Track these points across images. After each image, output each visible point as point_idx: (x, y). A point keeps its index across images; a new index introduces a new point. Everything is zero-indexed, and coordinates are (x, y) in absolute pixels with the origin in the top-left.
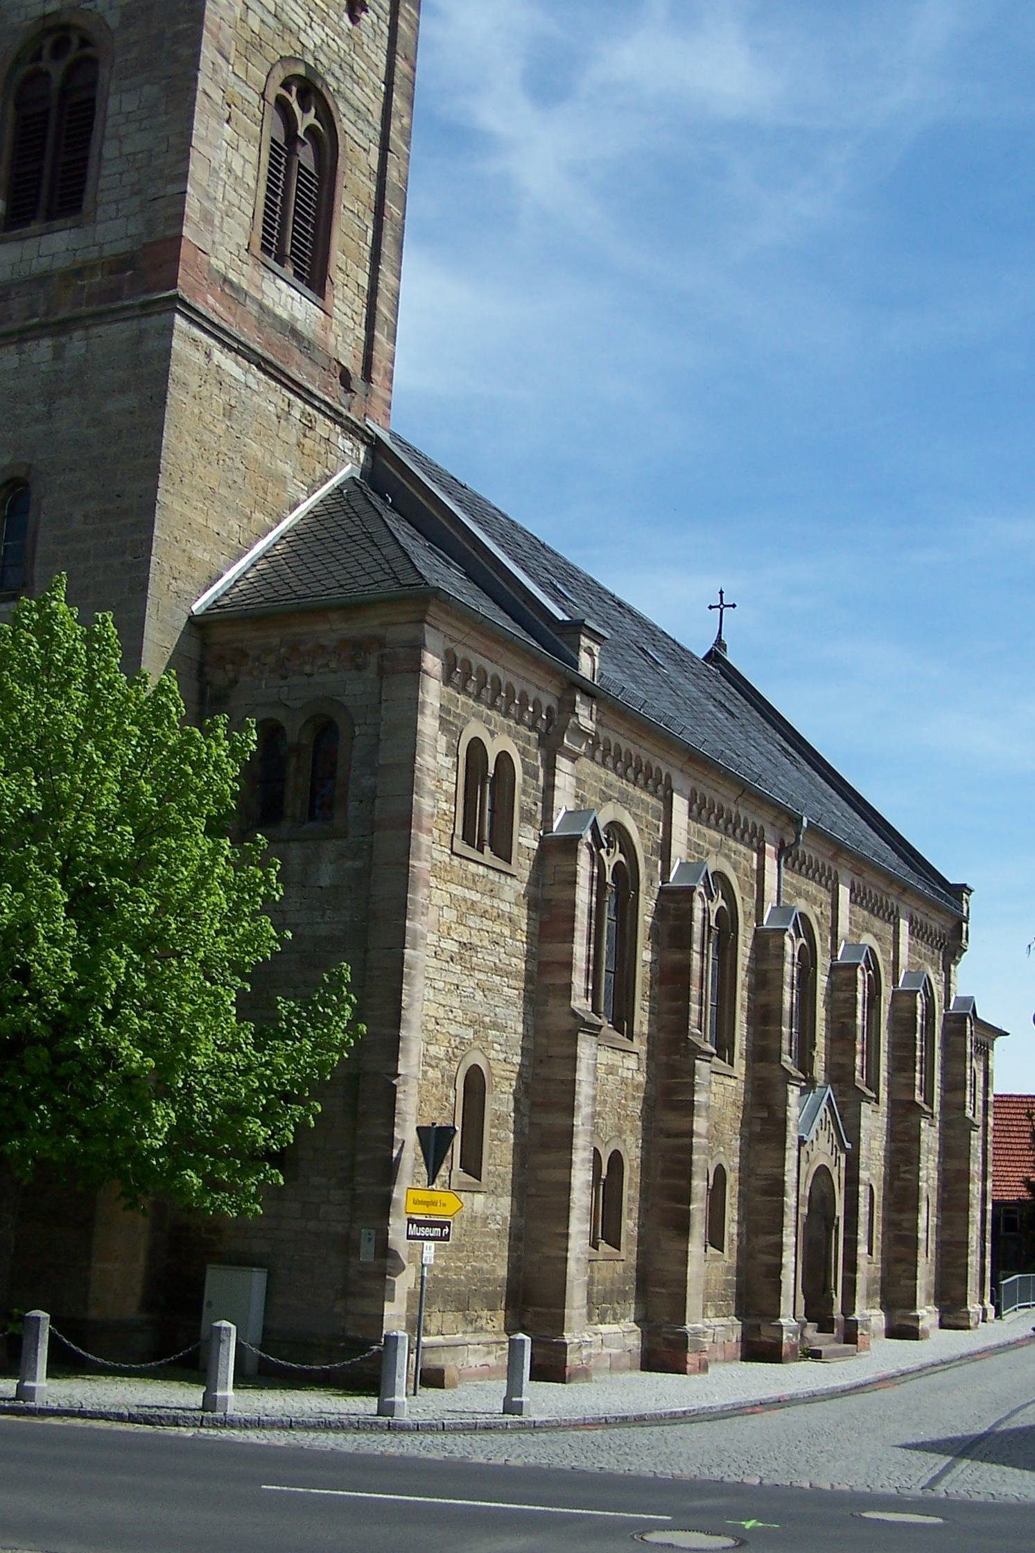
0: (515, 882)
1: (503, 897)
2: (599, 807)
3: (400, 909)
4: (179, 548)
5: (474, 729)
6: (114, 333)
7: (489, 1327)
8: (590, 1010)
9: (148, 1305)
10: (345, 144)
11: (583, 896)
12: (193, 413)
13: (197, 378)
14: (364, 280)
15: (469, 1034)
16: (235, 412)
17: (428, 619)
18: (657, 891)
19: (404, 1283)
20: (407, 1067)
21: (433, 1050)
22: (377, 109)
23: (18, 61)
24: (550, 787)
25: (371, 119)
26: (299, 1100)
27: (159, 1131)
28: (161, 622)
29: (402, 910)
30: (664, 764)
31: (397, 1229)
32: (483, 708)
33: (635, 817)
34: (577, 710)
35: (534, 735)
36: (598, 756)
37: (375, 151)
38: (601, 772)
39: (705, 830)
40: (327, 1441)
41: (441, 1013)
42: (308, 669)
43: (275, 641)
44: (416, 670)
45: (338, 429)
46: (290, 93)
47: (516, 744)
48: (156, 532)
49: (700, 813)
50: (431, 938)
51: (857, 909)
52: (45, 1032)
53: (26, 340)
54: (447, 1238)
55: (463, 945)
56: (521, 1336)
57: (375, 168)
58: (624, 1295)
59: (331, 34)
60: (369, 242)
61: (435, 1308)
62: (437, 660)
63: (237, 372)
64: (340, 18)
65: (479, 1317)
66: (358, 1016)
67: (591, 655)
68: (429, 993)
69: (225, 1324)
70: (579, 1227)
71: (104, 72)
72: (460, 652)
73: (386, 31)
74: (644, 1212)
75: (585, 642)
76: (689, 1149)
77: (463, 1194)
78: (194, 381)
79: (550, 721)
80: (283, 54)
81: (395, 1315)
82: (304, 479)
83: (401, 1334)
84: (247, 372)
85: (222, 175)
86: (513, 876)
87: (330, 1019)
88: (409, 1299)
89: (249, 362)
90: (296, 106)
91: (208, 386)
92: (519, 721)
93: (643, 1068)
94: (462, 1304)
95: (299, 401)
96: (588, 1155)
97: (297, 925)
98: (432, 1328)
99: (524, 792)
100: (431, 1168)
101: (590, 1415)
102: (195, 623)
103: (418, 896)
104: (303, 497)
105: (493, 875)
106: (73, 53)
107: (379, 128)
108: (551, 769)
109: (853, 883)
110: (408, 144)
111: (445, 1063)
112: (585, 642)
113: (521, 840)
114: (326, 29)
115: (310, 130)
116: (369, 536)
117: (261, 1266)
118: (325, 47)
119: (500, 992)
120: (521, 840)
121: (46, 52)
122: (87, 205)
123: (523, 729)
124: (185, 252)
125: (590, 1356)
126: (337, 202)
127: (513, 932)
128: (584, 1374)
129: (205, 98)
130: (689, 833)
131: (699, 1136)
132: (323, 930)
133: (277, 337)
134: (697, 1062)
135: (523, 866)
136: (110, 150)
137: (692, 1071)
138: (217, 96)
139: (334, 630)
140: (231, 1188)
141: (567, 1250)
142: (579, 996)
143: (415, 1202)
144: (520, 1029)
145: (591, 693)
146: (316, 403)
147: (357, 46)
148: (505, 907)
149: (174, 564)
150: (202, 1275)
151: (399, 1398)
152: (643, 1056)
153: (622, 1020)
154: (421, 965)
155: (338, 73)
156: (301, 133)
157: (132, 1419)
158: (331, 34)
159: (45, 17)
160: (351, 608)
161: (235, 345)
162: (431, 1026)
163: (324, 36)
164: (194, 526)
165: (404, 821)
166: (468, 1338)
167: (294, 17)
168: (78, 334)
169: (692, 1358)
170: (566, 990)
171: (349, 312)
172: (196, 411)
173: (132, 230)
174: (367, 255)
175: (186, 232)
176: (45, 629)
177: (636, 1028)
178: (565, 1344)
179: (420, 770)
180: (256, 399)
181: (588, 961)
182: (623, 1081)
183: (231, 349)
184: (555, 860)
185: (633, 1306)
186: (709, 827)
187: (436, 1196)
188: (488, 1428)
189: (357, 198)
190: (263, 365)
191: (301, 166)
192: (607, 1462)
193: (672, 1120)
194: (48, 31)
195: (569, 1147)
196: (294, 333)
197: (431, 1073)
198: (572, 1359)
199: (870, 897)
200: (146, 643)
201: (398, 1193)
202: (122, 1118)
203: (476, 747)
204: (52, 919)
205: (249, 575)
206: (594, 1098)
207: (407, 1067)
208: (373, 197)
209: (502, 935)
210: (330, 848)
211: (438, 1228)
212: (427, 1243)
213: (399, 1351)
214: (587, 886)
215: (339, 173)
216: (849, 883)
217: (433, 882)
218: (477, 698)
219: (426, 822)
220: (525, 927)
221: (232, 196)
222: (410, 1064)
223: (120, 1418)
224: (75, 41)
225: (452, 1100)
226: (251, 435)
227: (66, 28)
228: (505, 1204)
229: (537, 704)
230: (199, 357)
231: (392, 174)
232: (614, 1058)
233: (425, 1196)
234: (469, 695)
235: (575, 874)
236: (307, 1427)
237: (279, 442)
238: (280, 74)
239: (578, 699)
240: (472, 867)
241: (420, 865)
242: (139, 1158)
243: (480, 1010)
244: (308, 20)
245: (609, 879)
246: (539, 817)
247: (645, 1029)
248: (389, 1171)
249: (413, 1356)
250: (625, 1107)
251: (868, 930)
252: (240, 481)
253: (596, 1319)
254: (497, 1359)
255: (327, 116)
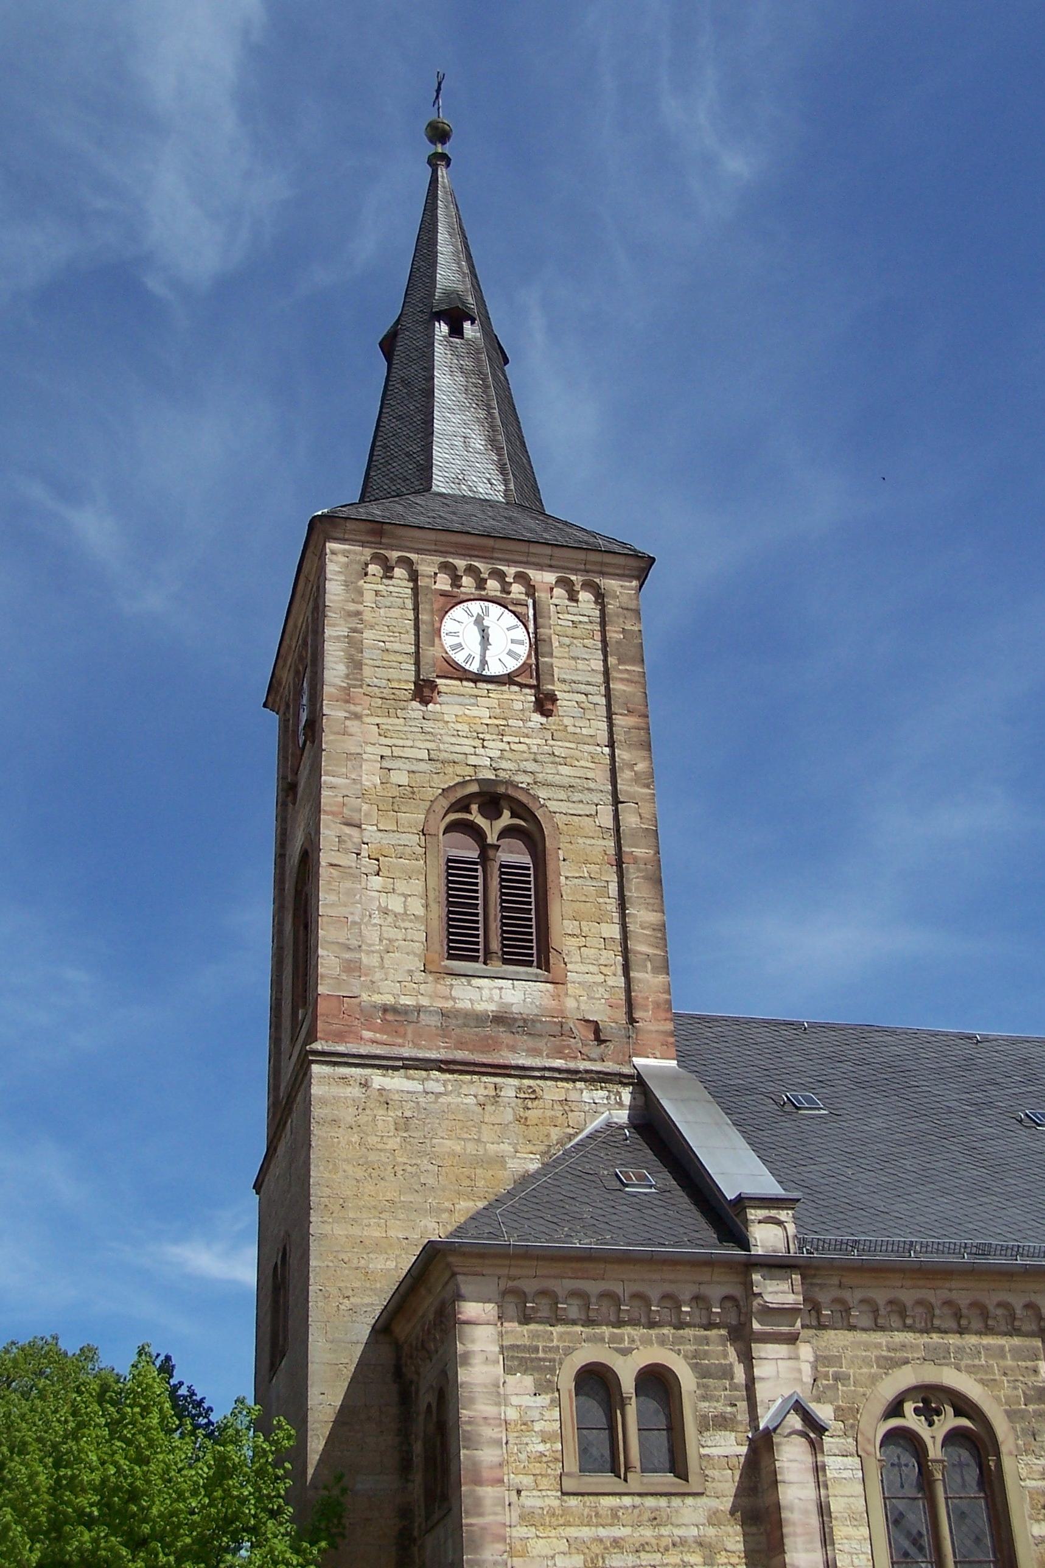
4: (350, 1268)
12: (349, 1143)
17: (456, 1269)
28: (332, 1342)
47: (679, 1352)
48: (313, 1263)
78: (348, 1115)
82: (534, 1149)
89: (426, 1070)
91: (368, 1112)
133: (469, 1033)
146: (537, 1074)
149: (342, 1285)
164: (367, 1242)
183: (396, 1068)
255: (521, 810)
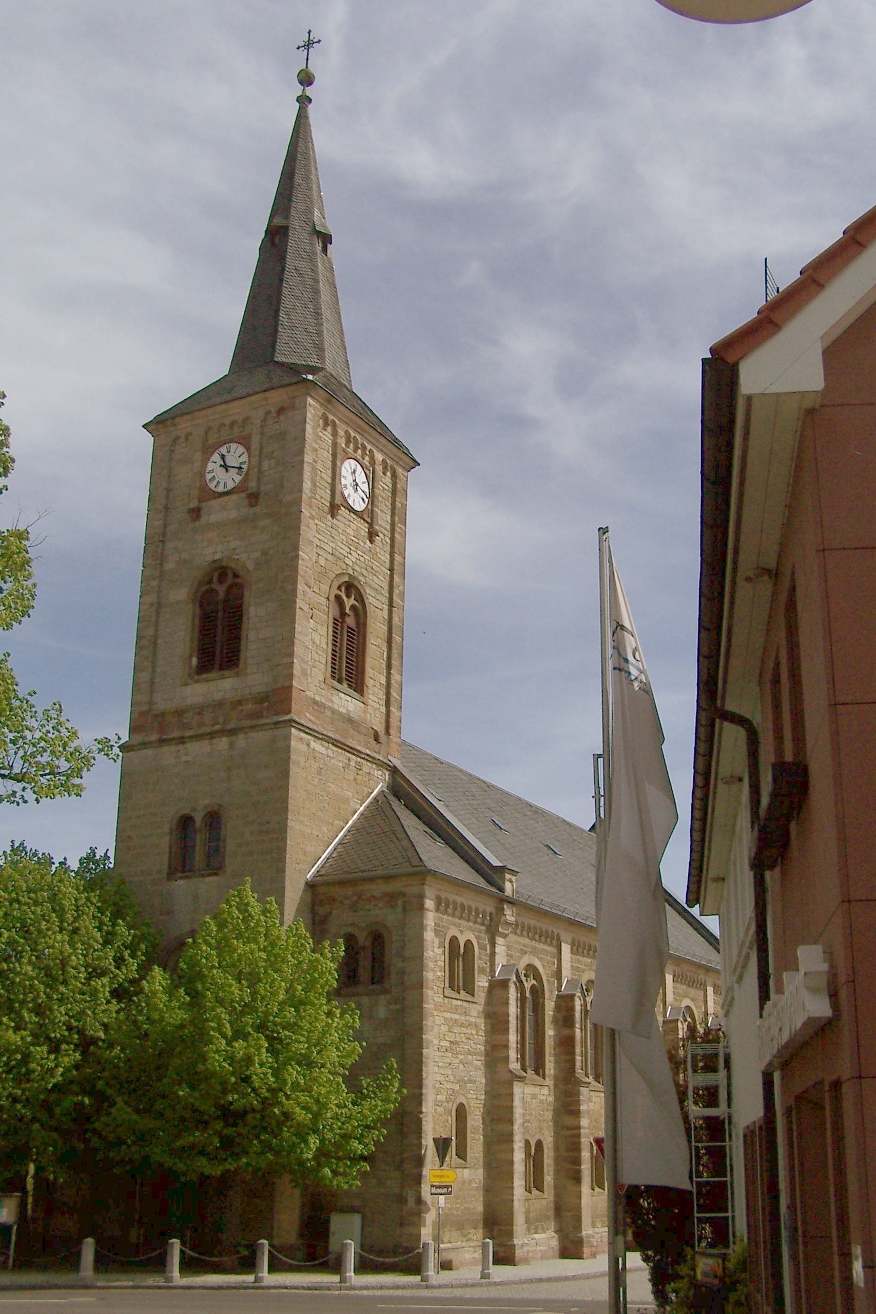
0: (477, 1006)
1: (472, 1014)
2: (520, 958)
3: (420, 1029)
5: (453, 932)
6: (260, 737)
7: (475, 1238)
8: (519, 1068)
9: (301, 1235)
10: (370, 610)
11: (513, 1010)
13: (303, 758)
14: (383, 680)
15: (457, 1087)
16: (323, 771)
18: (555, 997)
19: (430, 1217)
20: (426, 1108)
21: (439, 1097)
22: (386, 585)
23: (200, 585)
24: (493, 954)
25: (383, 592)
26: (375, 1128)
27: (311, 1150)
29: (420, 1030)
30: (554, 928)
31: (425, 1190)
32: (457, 920)
33: (540, 959)
34: (505, 913)
35: (484, 928)
36: (518, 931)
37: (386, 607)
38: (521, 940)
39: (581, 958)
40: (399, 1293)
41: (442, 1078)
42: (367, 907)
43: (350, 893)
44: (421, 908)
45: (374, 766)
46: (341, 591)
48: (288, 842)
49: (578, 950)
50: (436, 1042)
51: (678, 985)
52: (259, 1107)
53: (214, 738)
54: (450, 1193)
55: (451, 1042)
56: (487, 1240)
57: (386, 617)
58: (548, 1218)
59: (361, 554)
60: (385, 659)
61: (446, 1229)
62: (432, 902)
63: (323, 750)
64: (365, 543)
65: (470, 1233)
66: (402, 1084)
67: (511, 882)
68: (436, 1069)
69: (349, 1241)
70: (519, 1183)
71: (246, 593)
72: (443, 895)
73: (389, 541)
74: (557, 1172)
75: (508, 876)
76: (579, 1136)
77: (458, 1170)
78: (302, 759)
79: (491, 920)
80: (336, 573)
81: (426, 1233)
82: (359, 797)
83: (431, 1242)
84: (328, 748)
85: (310, 647)
86: (476, 1003)
87: (388, 1087)
88: (433, 1226)
90: (344, 597)
92: (475, 922)
93: (552, 1093)
94: (460, 1227)
95: (354, 757)
96: (522, 1144)
97: (368, 1038)
98: (445, 1240)
99: (480, 959)
100: (441, 1157)
101: (523, 1278)
102: (311, 886)
103: (428, 1022)
104: (358, 807)
105: (465, 1004)
106: (229, 581)
107: (388, 595)
108: (493, 944)
109: (674, 971)
110: (403, 601)
111: (445, 1104)
112: (508, 876)
113: (479, 983)
114: (358, 552)
115: (353, 607)
116: (394, 832)
117: (358, 1212)
118: (358, 562)
119: (472, 1064)
120: (479, 983)
121: (215, 579)
122: (241, 665)
123: (477, 926)
124: (295, 694)
125: (528, 1251)
126: (367, 642)
127: (477, 1032)
128: (526, 1261)
129: (300, 610)
130: (571, 962)
131: (584, 1128)
132: (380, 1040)
134: (581, 1088)
135: (481, 996)
136: (252, 636)
137: (578, 1094)
138: (306, 608)
139: (379, 888)
140: (344, 1174)
141: (513, 1195)
142: (513, 1062)
143: (434, 1176)
144: (483, 1081)
145: (511, 902)
147: (374, 555)
148: (473, 1020)
150: (328, 1221)
151: (431, 1273)
152: (552, 1087)
153: (539, 1069)
154: (431, 1056)
155: (365, 573)
156: (347, 611)
157: (309, 1288)
158: (361, 554)
159: (214, 561)
160: (389, 878)
161: (321, 737)
162: (438, 1085)
163: (357, 556)
165: (420, 985)
166: (464, 1244)
167: (342, 551)
168: (242, 736)
169: (586, 1251)
170: (506, 1059)
171: (376, 700)
172: (304, 775)
173: (266, 680)
174: (384, 666)
175: (294, 683)
176: (244, 907)
177: (547, 1072)
178: (514, 1246)
179: (426, 959)
180: (333, 761)
181: (517, 1043)
182: (541, 1102)
184: (498, 992)
185: (553, 1223)
186: (584, 956)
187: (444, 1172)
188: (473, 1285)
189: (378, 637)
190: (335, 743)
191: (349, 627)
192: (527, 1295)
193: (568, 1121)
194: (216, 570)
195: (512, 1141)
196: (350, 720)
197: (439, 1109)
198: (519, 1253)
199: (686, 977)
200: (286, 900)
201: (425, 1172)
202: (294, 1145)
203: (454, 941)
204: (260, 1054)
205: (334, 855)
206: (524, 1115)
207: (426, 1108)
208: (386, 634)
209: (472, 1034)
210: (383, 999)
211: (446, 1189)
212: (441, 1197)
213: (430, 1250)
214: (515, 1004)
215: (368, 626)
216: (672, 972)
217: (435, 1013)
218: (453, 915)
219: (431, 984)
220: (483, 1028)
221: (316, 657)
222: (428, 1107)
223: (303, 1288)
224: (230, 575)
225: (450, 1122)
226: (331, 781)
227: (226, 568)
228: (480, 1172)
229: (484, 912)
230: (304, 748)
231: (396, 619)
232: (536, 1090)
233: (439, 1173)
234: (449, 915)
235: (508, 999)
236: (388, 1288)
237: (345, 781)
238: (336, 584)
239: (505, 907)
240: (455, 1002)
241: (428, 1006)
242: (302, 1163)
243: (462, 1074)
244: (348, 550)
245: (528, 994)
246: (488, 970)
247: (552, 1072)
248: (419, 1161)
249: (436, 1254)
250: (543, 1116)
251: (686, 997)
252: (327, 806)
253: (532, 1231)
254: (478, 1255)
255: (360, 598)
